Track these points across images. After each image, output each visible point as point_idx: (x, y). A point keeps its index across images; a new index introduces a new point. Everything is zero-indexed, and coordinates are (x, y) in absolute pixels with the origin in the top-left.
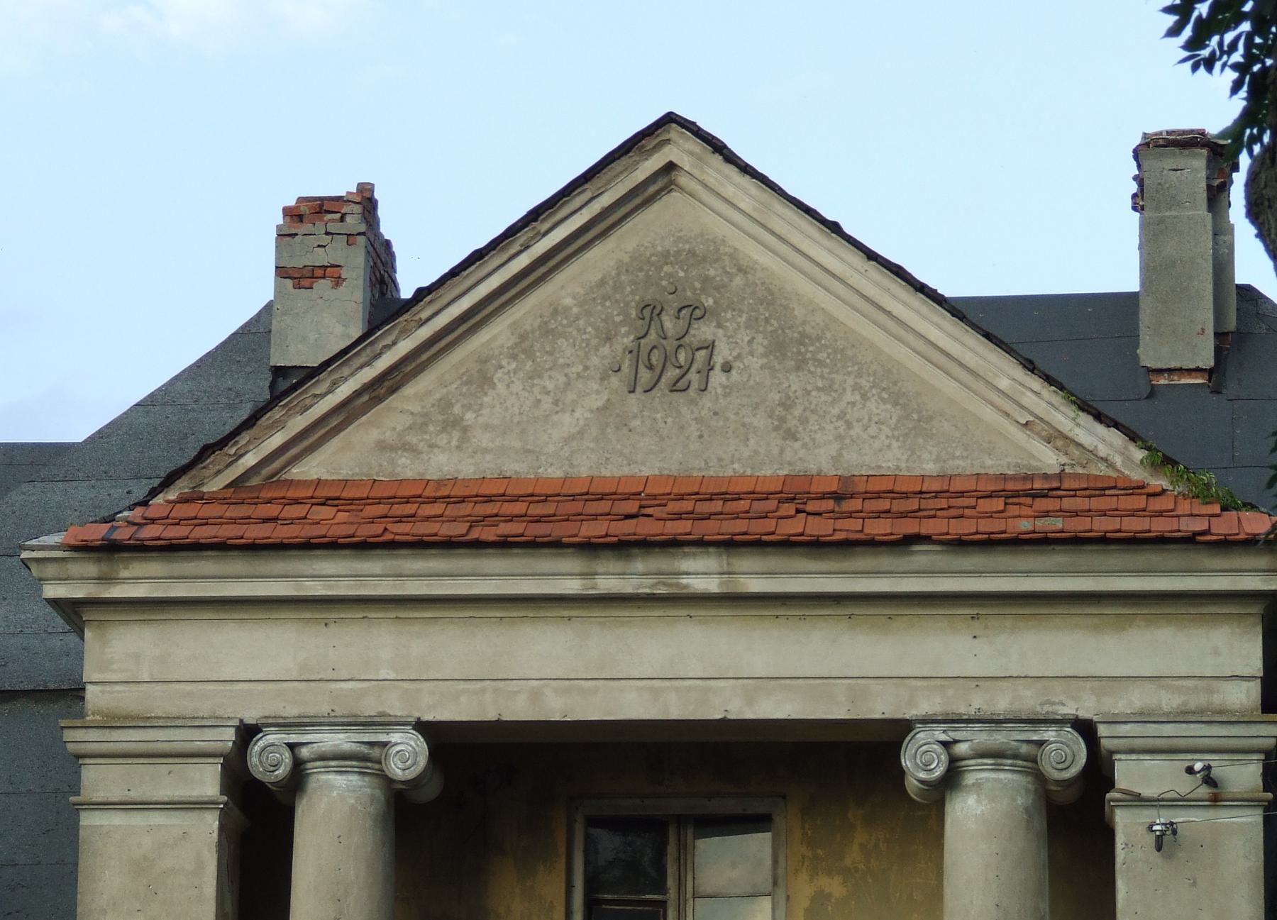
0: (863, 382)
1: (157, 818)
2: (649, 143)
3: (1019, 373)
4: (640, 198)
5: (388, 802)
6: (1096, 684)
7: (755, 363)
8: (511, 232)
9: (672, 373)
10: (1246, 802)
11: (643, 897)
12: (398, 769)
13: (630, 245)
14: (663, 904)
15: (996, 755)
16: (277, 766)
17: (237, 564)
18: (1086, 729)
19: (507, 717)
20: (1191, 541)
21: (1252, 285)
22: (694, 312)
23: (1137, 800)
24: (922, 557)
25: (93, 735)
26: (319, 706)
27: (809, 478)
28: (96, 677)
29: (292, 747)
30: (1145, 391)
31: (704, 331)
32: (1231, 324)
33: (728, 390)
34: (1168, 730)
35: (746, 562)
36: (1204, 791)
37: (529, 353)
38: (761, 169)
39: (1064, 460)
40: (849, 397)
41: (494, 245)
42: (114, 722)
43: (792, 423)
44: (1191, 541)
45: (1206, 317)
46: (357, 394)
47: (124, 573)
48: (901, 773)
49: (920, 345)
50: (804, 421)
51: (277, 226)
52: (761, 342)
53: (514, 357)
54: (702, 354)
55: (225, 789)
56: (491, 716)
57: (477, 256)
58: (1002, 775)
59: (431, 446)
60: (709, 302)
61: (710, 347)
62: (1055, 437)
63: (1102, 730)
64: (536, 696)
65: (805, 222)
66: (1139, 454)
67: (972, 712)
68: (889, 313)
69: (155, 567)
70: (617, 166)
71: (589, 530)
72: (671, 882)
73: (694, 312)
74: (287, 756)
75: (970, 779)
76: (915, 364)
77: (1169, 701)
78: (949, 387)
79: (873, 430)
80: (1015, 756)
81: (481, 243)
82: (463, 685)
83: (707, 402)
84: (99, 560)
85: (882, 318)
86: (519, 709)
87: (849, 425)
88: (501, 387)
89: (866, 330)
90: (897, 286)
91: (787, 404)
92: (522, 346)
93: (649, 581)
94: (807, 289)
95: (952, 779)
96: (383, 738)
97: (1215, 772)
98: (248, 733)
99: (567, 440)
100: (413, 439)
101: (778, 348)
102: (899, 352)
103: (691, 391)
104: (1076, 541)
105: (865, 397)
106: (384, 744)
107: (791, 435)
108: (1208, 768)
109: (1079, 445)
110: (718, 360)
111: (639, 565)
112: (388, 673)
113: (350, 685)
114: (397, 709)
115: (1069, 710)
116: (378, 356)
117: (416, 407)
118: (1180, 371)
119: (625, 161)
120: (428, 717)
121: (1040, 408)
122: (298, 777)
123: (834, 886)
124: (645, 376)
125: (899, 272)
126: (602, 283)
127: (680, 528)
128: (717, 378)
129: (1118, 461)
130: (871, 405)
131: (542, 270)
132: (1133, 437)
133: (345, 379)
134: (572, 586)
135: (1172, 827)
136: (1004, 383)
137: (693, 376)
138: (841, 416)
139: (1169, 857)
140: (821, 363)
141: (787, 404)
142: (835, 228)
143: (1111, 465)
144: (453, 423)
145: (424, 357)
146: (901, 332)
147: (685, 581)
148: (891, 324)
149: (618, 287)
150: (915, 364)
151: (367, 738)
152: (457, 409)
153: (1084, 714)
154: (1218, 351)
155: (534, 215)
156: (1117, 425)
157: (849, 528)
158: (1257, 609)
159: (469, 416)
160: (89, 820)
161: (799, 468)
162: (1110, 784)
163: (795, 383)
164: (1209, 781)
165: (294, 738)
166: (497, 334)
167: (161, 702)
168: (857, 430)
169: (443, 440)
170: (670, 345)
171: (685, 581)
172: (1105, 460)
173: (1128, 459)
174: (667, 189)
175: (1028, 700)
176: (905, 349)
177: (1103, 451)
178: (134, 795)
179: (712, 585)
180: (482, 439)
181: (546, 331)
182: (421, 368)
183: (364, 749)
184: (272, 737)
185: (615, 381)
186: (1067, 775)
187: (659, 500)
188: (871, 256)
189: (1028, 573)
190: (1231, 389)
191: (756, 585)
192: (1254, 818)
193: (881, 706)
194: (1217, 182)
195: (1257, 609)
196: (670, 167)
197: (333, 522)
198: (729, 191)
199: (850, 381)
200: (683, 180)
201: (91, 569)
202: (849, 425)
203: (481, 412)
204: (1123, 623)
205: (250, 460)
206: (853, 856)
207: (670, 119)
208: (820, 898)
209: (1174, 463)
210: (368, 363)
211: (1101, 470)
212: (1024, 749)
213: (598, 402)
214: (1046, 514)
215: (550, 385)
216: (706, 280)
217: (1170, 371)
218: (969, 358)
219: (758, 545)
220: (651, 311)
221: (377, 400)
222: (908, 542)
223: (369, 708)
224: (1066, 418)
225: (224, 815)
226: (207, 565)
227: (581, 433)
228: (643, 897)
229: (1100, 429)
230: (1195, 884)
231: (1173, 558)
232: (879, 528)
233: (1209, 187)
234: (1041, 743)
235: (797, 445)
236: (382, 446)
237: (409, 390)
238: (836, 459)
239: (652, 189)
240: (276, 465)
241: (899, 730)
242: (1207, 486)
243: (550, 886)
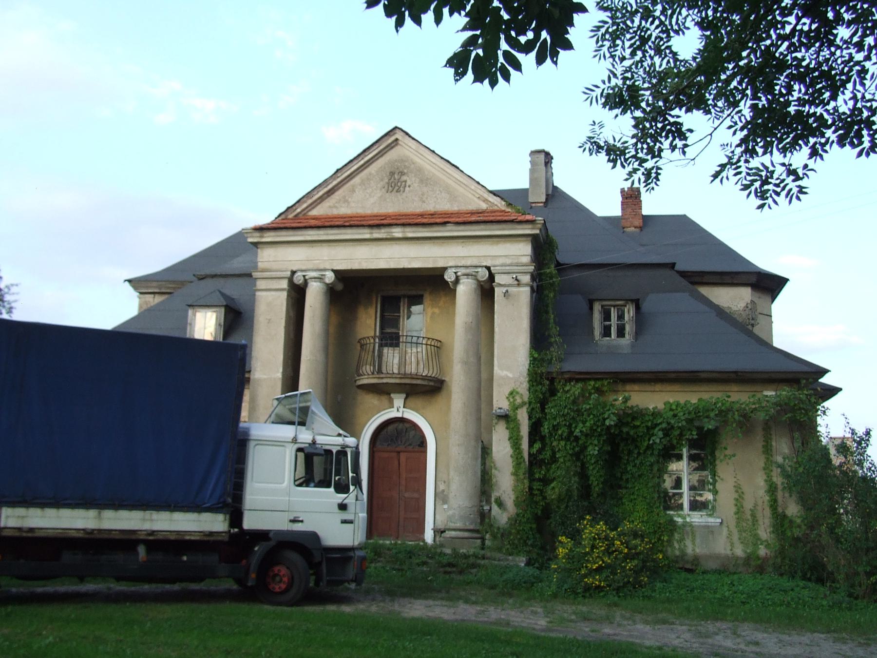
0: (441, 189)
1: (273, 293)
2: (391, 133)
4: (390, 147)
5: (327, 290)
6: (491, 258)
7: (416, 185)
8: (359, 155)
9: (397, 188)
10: (526, 285)
11: (706, 396)
12: (328, 281)
13: (388, 159)
14: (399, 316)
15: (467, 275)
16: (300, 280)
17: (291, 232)
18: (488, 268)
19: (354, 268)
20: (512, 221)
22: (402, 173)
23: (500, 285)
24: (449, 227)
25: (260, 273)
26: (310, 266)
27: (427, 211)
28: (261, 260)
29: (304, 276)
30: (530, 207)
31: (404, 178)
32: (550, 192)
33: (409, 192)
34: (508, 268)
35: (408, 229)
36: (516, 282)
37: (364, 184)
38: (419, 141)
39: (487, 206)
40: (438, 192)
41: (355, 158)
42: (263, 271)
43: (424, 199)
44: (512, 221)
45: (544, 191)
46: (324, 195)
47: (265, 235)
48: (447, 282)
49: (454, 179)
50: (427, 198)
52: (418, 180)
53: (360, 185)
54: (404, 183)
55: (288, 286)
56: (349, 268)
57: (351, 161)
58: (469, 280)
59: (341, 206)
60: (406, 171)
61: (406, 181)
62: (485, 201)
63: (492, 268)
64: (360, 263)
65: (427, 150)
66: (504, 203)
67: (462, 265)
68: (446, 172)
69: (272, 233)
70: (384, 139)
71: (371, 222)
72: (401, 311)
73: (402, 173)
74: (302, 278)
75: (461, 281)
76: (453, 184)
77: (508, 261)
78: (461, 190)
79: (443, 200)
80: (472, 275)
81: (352, 158)
82: (343, 261)
83: (404, 194)
84: (259, 232)
85: (445, 173)
86: (356, 266)
87: (437, 199)
88: (357, 192)
89: (444, 178)
90: (448, 165)
91: (423, 195)
92: (362, 183)
93: (386, 234)
94: (428, 167)
95: (457, 281)
96: (324, 273)
97: (518, 278)
98: (293, 273)
99: (372, 204)
100: (337, 205)
101: (421, 181)
102: (450, 182)
103: (401, 192)
105: (441, 192)
106: (324, 275)
107: (424, 202)
108: (516, 277)
109: (490, 202)
110: (407, 185)
111: (383, 231)
112: (729, 397)
113: (318, 261)
114: (328, 267)
115: (484, 264)
116: (329, 185)
117: (337, 198)
118: (538, 203)
119: (386, 138)
120: (335, 268)
121: (481, 193)
122: (306, 282)
123: (437, 310)
124: (390, 189)
125: (448, 161)
126: (381, 167)
127: (391, 222)
128: (407, 189)
129: (499, 205)
130: (443, 194)
131: (367, 164)
132: (502, 199)
133: (320, 191)
134: (367, 236)
135: (507, 291)
136: (473, 187)
137: (402, 189)
138: (436, 197)
139: (507, 299)
140: (431, 185)
141: (423, 195)
142: (433, 152)
143: (498, 207)
145: (340, 185)
146: (450, 177)
147: (394, 234)
148: (448, 175)
149: (385, 168)
150: (453, 184)
151: (322, 273)
152: (347, 198)
153: (488, 265)
154: (547, 199)
155: (365, 151)
156: (499, 196)
157: (432, 221)
158: (530, 239)
159: (350, 199)
160: (258, 294)
161: (425, 210)
162: (494, 281)
163: (425, 189)
164: (517, 280)
165: (304, 274)
166: (357, 180)
167: (275, 266)
168: (439, 200)
169: (343, 205)
170: (396, 181)
171: (394, 234)
172: (496, 205)
173: (501, 204)
174: (397, 144)
175: (475, 262)
176: (451, 181)
177: (496, 203)
178: (268, 288)
179: (400, 235)
180: (353, 205)
181: (368, 179)
182: (339, 188)
183: (320, 276)
184: (299, 274)
185: (383, 190)
186: (485, 279)
187: (390, 216)
188: (442, 158)
189: (474, 230)
190: (549, 206)
191: (410, 235)
193: (440, 264)
194: (547, 161)
195: (530, 239)
196: (397, 140)
197: (313, 223)
198: (410, 144)
199: (438, 189)
200: (400, 142)
201: (257, 234)
202: (437, 199)
204: (498, 243)
205: (299, 210)
206: (441, 303)
207: (396, 128)
208: (433, 313)
209: (511, 205)
210: (326, 187)
211: (496, 208)
212: (474, 273)
213: (379, 195)
214: (479, 217)
215: (368, 191)
216: (405, 166)
217: (535, 203)
218: (464, 182)
219: (410, 225)
220: (392, 174)
221: (329, 196)
222: (445, 223)
223: (322, 267)
225: (289, 292)
226: (284, 233)
227: (375, 203)
228: (706, 396)
229: (495, 197)
230: (513, 305)
231: (510, 226)
232: (438, 221)
233: (545, 162)
234: (477, 272)
235: (425, 204)
236: (330, 207)
237: (337, 193)
238: (434, 207)
239: (393, 145)
240: (305, 212)
241: (445, 269)
242: (519, 210)
243: (372, 311)
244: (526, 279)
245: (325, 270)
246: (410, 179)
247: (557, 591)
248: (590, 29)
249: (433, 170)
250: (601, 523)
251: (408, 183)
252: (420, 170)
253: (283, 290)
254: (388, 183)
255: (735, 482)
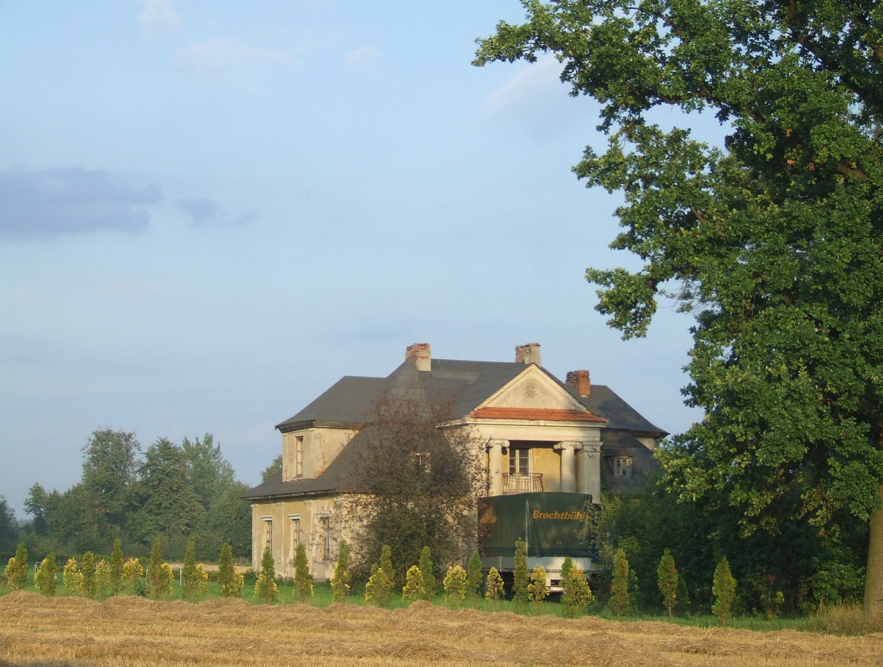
3: (572, 397)
21: (347, 375)
22: (533, 387)
31: (534, 390)
51: (587, 372)
61: (535, 392)
66: (585, 409)
73: (533, 387)
104: (591, 421)
107: (544, 404)
128: (536, 396)
144: (505, 400)
192: (599, 454)
203: (849, 462)
220: (528, 387)
224: (578, 404)
244: (598, 449)
245: (504, 440)
246: (537, 391)
247: (812, 238)
248: (613, 238)
249: (548, 387)
250: (871, 136)
251: (536, 393)
252: (542, 387)
253: (543, 489)
254: (526, 392)
255: (468, 626)
